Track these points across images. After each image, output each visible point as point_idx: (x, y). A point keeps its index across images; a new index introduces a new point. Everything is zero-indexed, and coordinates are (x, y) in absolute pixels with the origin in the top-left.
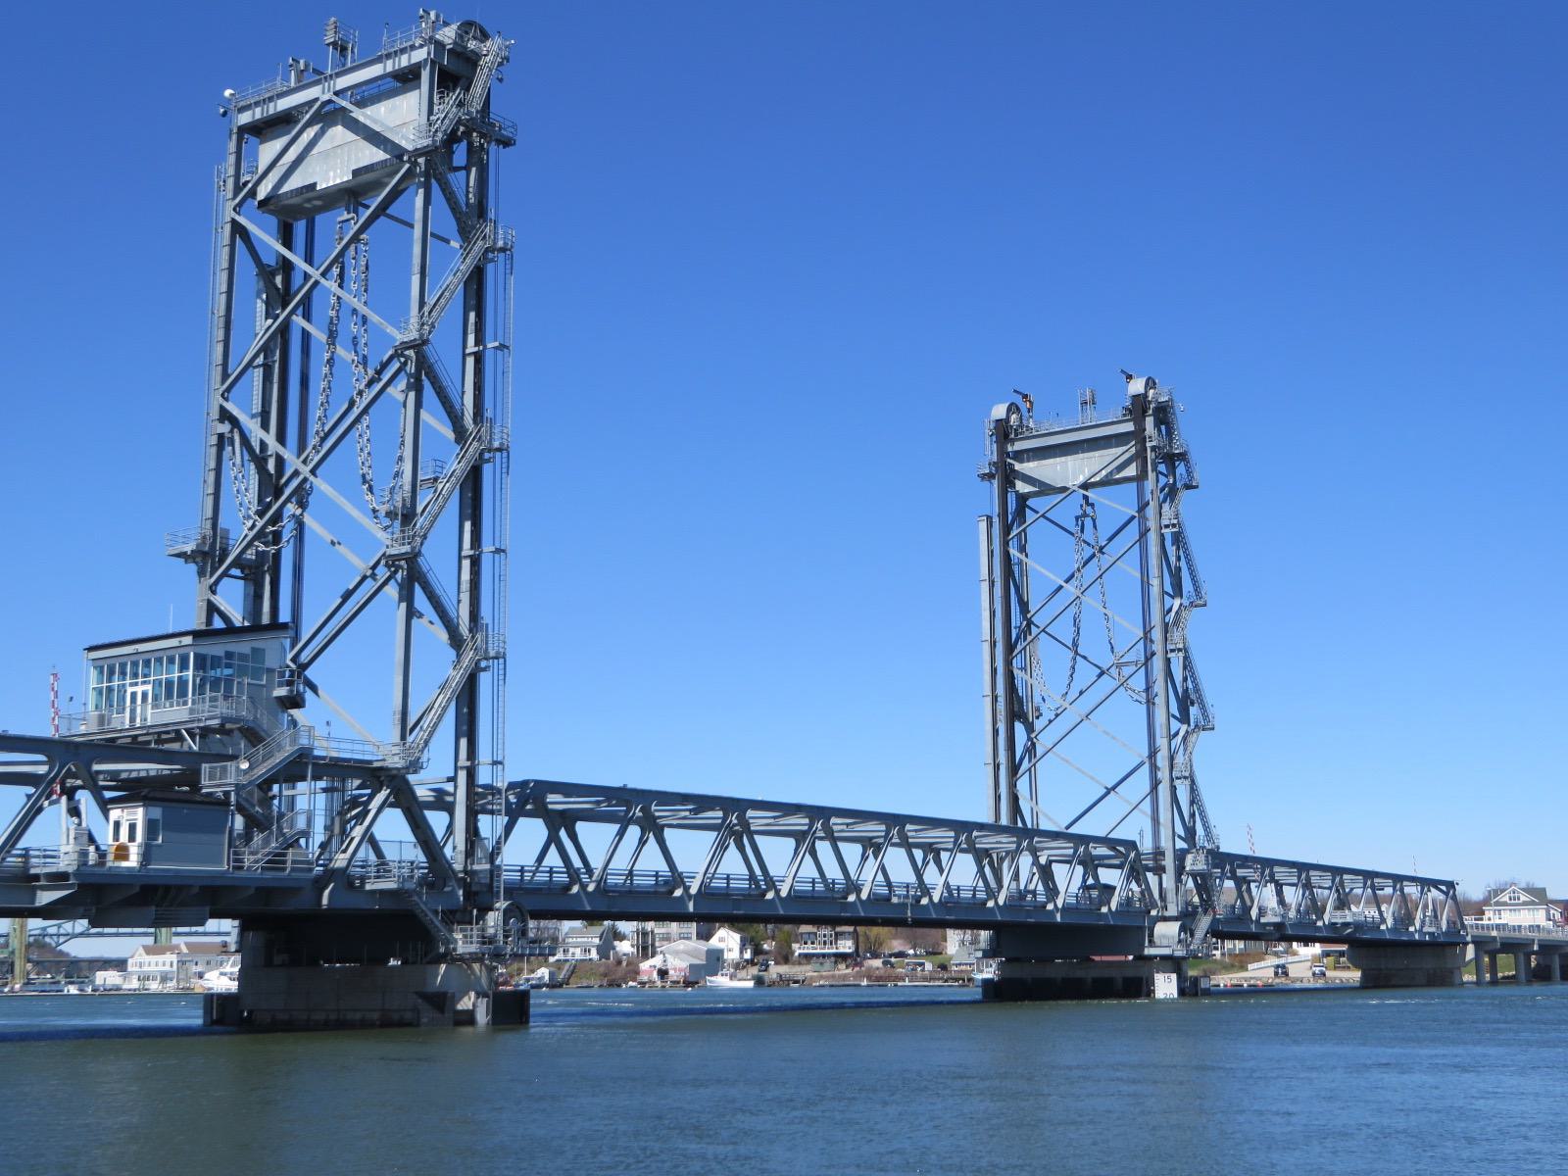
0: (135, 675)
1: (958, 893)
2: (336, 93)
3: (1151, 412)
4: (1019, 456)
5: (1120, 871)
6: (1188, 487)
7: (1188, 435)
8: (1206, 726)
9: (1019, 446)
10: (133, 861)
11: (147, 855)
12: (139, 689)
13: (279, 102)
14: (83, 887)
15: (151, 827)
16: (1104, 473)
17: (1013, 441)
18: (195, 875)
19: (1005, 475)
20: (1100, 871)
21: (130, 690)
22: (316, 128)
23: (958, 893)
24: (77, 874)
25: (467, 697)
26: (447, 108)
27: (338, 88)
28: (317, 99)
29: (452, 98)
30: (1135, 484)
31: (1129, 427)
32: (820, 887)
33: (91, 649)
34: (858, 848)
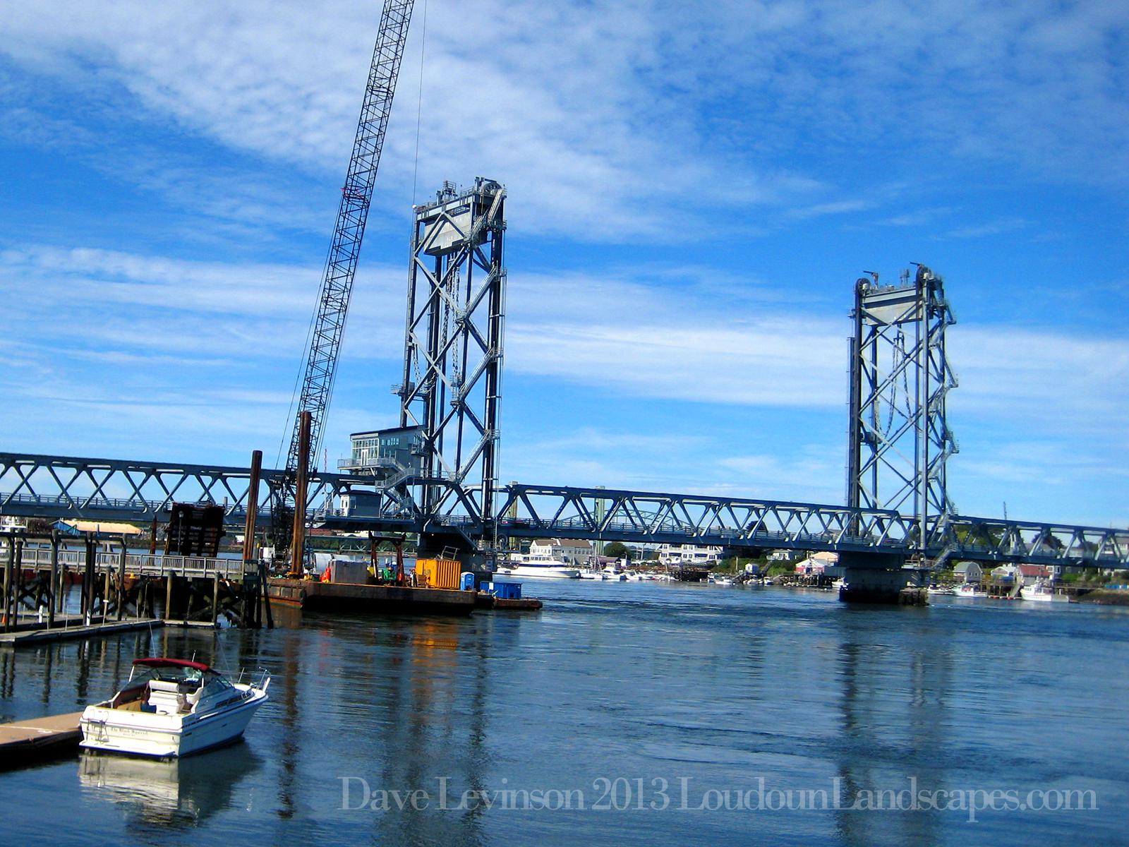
0: (363, 446)
1: (152, 505)
2: (447, 212)
3: (925, 285)
4: (868, 306)
5: (1021, 531)
6: (950, 323)
7: (952, 296)
8: (954, 450)
9: (867, 301)
10: (346, 514)
11: (351, 512)
12: (365, 451)
13: (430, 212)
14: (327, 523)
15: (352, 503)
16: (905, 316)
17: (865, 298)
18: (368, 520)
19: (859, 315)
20: (1085, 536)
21: (362, 451)
22: (442, 221)
23: (152, 505)
24: (326, 518)
25: (488, 450)
26: (479, 221)
27: (447, 209)
28: (440, 214)
29: (481, 218)
30: (915, 322)
31: (913, 293)
32: (34, 500)
33: (352, 435)
34: (828, 516)
